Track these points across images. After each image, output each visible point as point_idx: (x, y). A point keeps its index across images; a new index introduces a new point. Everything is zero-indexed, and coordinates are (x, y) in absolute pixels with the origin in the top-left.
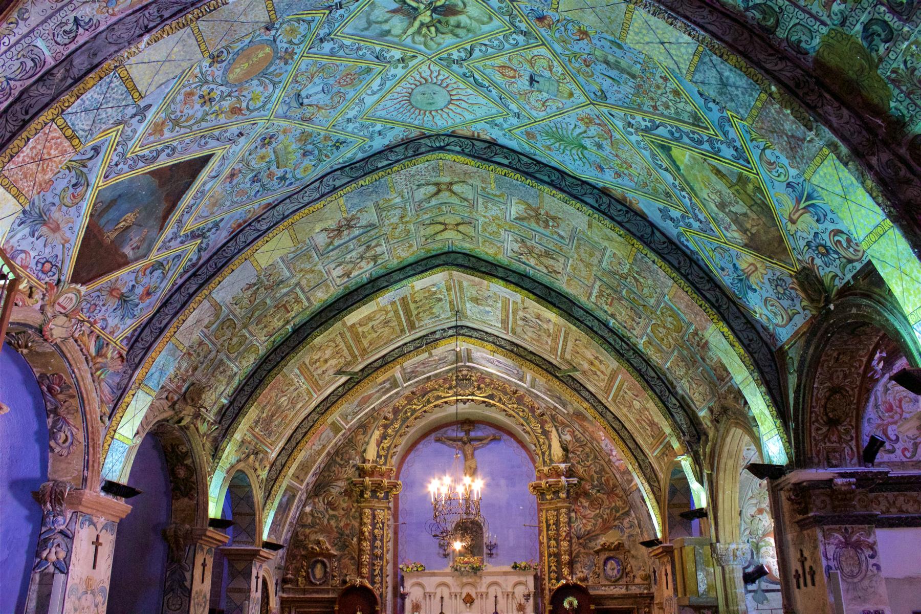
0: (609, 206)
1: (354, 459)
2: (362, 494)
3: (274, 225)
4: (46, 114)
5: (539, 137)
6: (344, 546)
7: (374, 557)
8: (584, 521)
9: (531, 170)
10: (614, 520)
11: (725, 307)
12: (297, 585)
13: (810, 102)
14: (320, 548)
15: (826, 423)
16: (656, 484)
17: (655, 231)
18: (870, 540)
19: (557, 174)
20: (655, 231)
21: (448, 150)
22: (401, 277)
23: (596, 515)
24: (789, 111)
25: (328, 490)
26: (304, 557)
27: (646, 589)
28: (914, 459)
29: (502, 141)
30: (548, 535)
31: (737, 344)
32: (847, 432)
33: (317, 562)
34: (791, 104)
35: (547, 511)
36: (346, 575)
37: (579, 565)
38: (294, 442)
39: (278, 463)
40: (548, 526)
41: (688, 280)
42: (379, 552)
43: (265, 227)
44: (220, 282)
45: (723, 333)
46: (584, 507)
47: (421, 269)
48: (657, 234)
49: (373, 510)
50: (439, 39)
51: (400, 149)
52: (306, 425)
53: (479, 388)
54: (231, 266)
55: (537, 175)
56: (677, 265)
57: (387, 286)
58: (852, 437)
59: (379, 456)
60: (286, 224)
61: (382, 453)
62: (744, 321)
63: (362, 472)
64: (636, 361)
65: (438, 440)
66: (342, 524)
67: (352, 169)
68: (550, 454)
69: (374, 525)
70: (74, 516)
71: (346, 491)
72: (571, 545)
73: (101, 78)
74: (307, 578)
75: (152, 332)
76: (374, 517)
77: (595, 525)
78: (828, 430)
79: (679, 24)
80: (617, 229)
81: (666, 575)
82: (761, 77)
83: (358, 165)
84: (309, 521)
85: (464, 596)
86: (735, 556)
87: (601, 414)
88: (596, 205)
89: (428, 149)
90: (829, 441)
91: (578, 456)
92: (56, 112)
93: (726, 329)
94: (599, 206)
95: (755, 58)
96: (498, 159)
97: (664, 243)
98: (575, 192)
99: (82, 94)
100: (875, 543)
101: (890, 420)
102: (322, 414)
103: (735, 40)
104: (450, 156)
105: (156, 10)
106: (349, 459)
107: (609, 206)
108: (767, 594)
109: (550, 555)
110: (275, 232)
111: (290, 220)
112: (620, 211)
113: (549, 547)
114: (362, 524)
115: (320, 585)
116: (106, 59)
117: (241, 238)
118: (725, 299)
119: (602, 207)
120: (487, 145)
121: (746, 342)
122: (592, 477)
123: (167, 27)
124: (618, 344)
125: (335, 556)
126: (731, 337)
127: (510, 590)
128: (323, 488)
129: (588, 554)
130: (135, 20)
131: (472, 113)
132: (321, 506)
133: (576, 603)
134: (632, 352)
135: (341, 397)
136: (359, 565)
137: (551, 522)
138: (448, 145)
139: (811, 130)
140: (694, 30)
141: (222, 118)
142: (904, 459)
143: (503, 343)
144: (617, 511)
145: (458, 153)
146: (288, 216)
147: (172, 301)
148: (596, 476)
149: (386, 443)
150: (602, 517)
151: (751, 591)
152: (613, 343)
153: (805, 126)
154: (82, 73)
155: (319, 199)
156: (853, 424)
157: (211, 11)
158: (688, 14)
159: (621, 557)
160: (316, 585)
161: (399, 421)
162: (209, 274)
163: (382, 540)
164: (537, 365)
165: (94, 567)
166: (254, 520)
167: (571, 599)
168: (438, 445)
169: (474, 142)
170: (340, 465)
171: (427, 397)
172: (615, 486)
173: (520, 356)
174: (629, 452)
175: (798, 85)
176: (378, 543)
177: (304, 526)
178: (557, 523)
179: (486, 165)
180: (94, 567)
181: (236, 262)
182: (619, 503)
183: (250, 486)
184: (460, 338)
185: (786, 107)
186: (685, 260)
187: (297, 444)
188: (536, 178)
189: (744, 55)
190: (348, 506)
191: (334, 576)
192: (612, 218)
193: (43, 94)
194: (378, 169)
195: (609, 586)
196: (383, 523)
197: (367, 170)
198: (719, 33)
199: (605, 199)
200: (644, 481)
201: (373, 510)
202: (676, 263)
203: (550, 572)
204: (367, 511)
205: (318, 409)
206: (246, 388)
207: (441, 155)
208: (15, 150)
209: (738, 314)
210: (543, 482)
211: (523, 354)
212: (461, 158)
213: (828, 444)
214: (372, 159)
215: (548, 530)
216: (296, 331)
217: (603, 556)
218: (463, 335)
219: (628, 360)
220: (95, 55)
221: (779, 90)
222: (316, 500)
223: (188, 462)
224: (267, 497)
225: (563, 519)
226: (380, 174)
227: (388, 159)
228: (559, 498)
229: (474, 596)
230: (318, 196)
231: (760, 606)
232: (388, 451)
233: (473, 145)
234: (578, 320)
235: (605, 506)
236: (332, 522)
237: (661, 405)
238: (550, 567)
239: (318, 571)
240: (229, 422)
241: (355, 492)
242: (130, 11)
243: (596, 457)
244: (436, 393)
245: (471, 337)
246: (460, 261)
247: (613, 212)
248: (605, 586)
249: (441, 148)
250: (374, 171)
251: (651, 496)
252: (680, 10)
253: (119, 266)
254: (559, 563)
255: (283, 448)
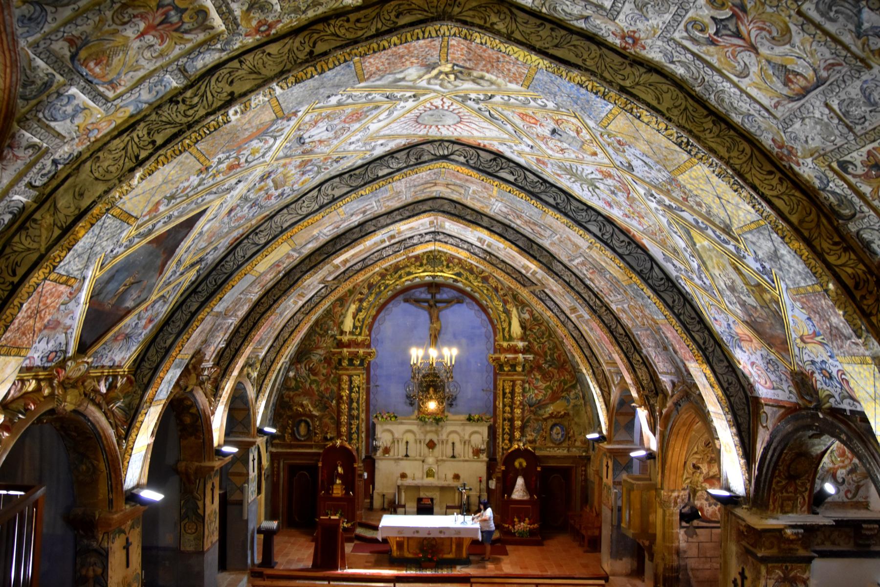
0: (612, 235)
1: (332, 330)
2: (340, 362)
3: (273, 239)
4: (36, 275)
5: (549, 166)
6: (325, 407)
7: (351, 417)
8: (536, 391)
9: (537, 190)
10: (562, 391)
11: (710, 349)
12: (284, 440)
13: (865, 307)
14: (304, 409)
15: (787, 478)
16: (606, 389)
17: (654, 266)
18: (805, 576)
19: (563, 196)
20: (654, 266)
21: (453, 160)
22: (388, 221)
23: (547, 387)
24: (841, 312)
25: (310, 357)
26: (290, 417)
27: (584, 451)
28: (855, 500)
29: (508, 153)
30: (503, 401)
31: (717, 386)
32: (803, 484)
33: (301, 421)
34: (845, 307)
35: (504, 381)
36: (327, 433)
37: (529, 429)
38: (281, 340)
39: (267, 359)
40: (504, 394)
41: (680, 320)
42: (355, 413)
43: (263, 241)
44: (221, 299)
45: (705, 374)
46: (536, 379)
47: (408, 214)
48: (656, 269)
49: (350, 376)
50: (458, 82)
51: (402, 155)
52: (292, 324)
53: (448, 267)
54: (231, 283)
55: (543, 197)
56: (671, 304)
57: (375, 231)
58: (806, 489)
59: (355, 327)
60: (284, 237)
61: (357, 324)
62: (726, 363)
63: (340, 344)
64: (607, 318)
65: (406, 301)
66: (322, 388)
67: (351, 176)
68: (509, 331)
69: (351, 390)
70: (106, 537)
71: (325, 358)
72: (523, 412)
73: (92, 225)
74: (293, 434)
75: (157, 351)
76: (351, 382)
77: (545, 395)
78: (787, 484)
79: (744, 194)
80: (617, 261)
81: (607, 466)
82: (820, 271)
83: (357, 172)
84: (293, 384)
85: (427, 441)
86: (676, 503)
87: (562, 323)
88: (599, 234)
89: (431, 157)
90: (787, 492)
91: (535, 333)
92: (47, 271)
93: (708, 372)
94: (603, 235)
95: (818, 248)
96: (503, 174)
97: (662, 279)
98: (579, 218)
99: (73, 245)
100: (808, 578)
101: (841, 464)
102: (307, 314)
103: (801, 222)
104: (452, 166)
105: (145, 132)
106: (328, 330)
107: (612, 235)
108: (698, 530)
109: (504, 420)
110: (274, 246)
111: (289, 234)
112: (622, 242)
113: (504, 412)
114: (340, 388)
115: (305, 441)
116: (94, 203)
117: (239, 252)
118: (712, 342)
119: (605, 237)
120: (493, 156)
121: (725, 385)
122: (545, 353)
123: (162, 158)
124: (593, 300)
125: (316, 416)
126: (713, 379)
127: (467, 437)
128: (305, 355)
129: (537, 420)
130: (122, 145)
131: (480, 132)
132: (303, 371)
133: (524, 464)
134: (604, 308)
135: (324, 298)
136: (338, 424)
137: (507, 391)
138: (452, 154)
139: (859, 337)
140: (760, 204)
141: (220, 177)
142: (846, 500)
143: (477, 250)
144: (565, 384)
145: (462, 164)
146: (286, 229)
147: (174, 319)
148: (549, 352)
149: (361, 316)
150: (552, 389)
151: (684, 527)
152: (587, 299)
153: (855, 332)
154: (70, 220)
155: (317, 210)
156: (810, 479)
157: (211, 133)
158: (757, 182)
159: (566, 423)
160: (301, 441)
161: (373, 296)
162: (210, 291)
163: (358, 402)
164: (508, 274)
165: (128, 566)
166: (249, 415)
167: (521, 460)
168: (407, 305)
169: (480, 152)
170: (319, 334)
171: (399, 273)
172: (565, 362)
173: (492, 264)
174: (585, 359)
175: (857, 286)
176: (355, 405)
177: (288, 389)
178: (513, 392)
179: (490, 179)
180: (128, 566)
181: (236, 279)
182: (568, 377)
183: (245, 389)
184: (437, 243)
185: (839, 308)
186: (679, 299)
187: (284, 342)
188: (541, 200)
189: (808, 242)
190: (327, 373)
191: (316, 434)
192: (613, 250)
193: (29, 249)
194: (378, 178)
195: (553, 448)
196: (359, 387)
197: (367, 179)
198: (785, 209)
199: (609, 228)
200: (596, 386)
201: (350, 376)
202: (670, 302)
203: (503, 434)
204: (345, 378)
205: (303, 310)
206: (241, 330)
207: (445, 164)
208: (9, 320)
209: (722, 357)
210: (502, 357)
211: (495, 262)
212: (465, 170)
213: (785, 494)
214: (372, 166)
215: (504, 397)
216: (288, 274)
217: (550, 423)
218: (439, 241)
219: (600, 317)
220: (81, 195)
221: (837, 289)
222: (299, 366)
223: (193, 411)
224: (259, 392)
225: (518, 389)
226: (381, 184)
227: (389, 167)
228: (515, 371)
229: (436, 441)
230: (317, 207)
231: (690, 540)
232: (363, 322)
233: (479, 155)
234: (557, 275)
235: (555, 379)
236: (314, 386)
237: (625, 360)
238: (503, 429)
239: (303, 429)
240: (227, 363)
241: (334, 362)
242: (116, 133)
243: (550, 335)
244: (407, 270)
245: (446, 243)
246: (447, 207)
247: (616, 243)
248: (550, 447)
249: (444, 157)
250: (374, 180)
251: (601, 399)
252: (748, 176)
253: (121, 318)
254: (512, 426)
255: (272, 346)
